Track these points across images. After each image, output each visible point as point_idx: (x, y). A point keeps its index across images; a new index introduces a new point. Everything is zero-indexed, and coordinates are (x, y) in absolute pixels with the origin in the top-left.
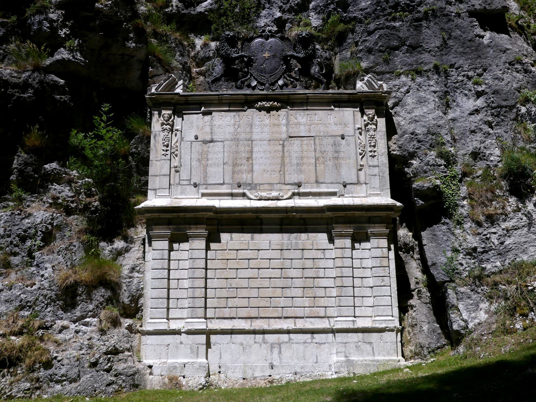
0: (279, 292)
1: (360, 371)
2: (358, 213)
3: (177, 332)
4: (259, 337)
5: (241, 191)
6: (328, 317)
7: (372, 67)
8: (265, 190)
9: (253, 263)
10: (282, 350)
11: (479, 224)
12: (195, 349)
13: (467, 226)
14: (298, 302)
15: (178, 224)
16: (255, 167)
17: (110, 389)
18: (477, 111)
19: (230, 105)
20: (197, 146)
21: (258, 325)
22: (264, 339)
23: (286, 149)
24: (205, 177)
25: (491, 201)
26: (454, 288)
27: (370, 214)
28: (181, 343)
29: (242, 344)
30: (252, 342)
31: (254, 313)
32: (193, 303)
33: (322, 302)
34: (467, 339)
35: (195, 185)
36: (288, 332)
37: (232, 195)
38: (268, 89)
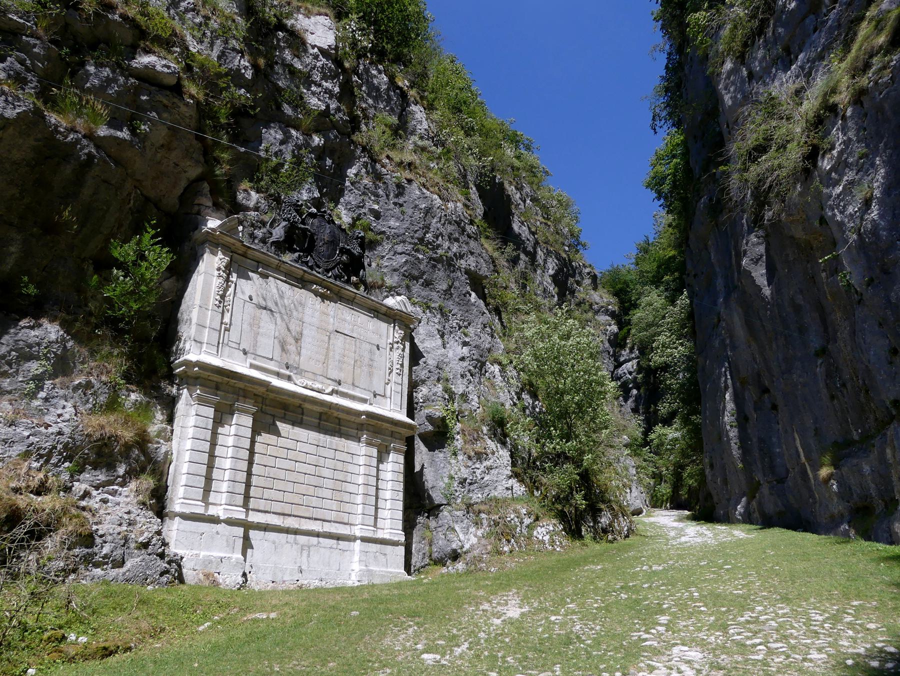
0: (311, 491)
1: (377, 581)
2: (386, 425)
3: (214, 520)
4: (291, 537)
5: (287, 372)
6: (351, 525)
7: (395, 287)
8: (309, 379)
9: (291, 455)
10: (311, 553)
11: (470, 458)
12: (231, 543)
13: (460, 457)
14: (327, 504)
15: (227, 392)
16: (303, 351)
17: (164, 579)
18: (462, 359)
19: (286, 275)
20: (250, 307)
21: (291, 523)
22: (295, 539)
23: (331, 341)
24: (255, 345)
25: (476, 440)
26: (450, 512)
27: (395, 429)
28: (218, 533)
29: (274, 543)
30: (284, 541)
31: (287, 509)
32: (234, 487)
33: (347, 508)
34: (468, 557)
35: (245, 353)
36: (318, 535)
37: (278, 375)
38: (323, 274)
